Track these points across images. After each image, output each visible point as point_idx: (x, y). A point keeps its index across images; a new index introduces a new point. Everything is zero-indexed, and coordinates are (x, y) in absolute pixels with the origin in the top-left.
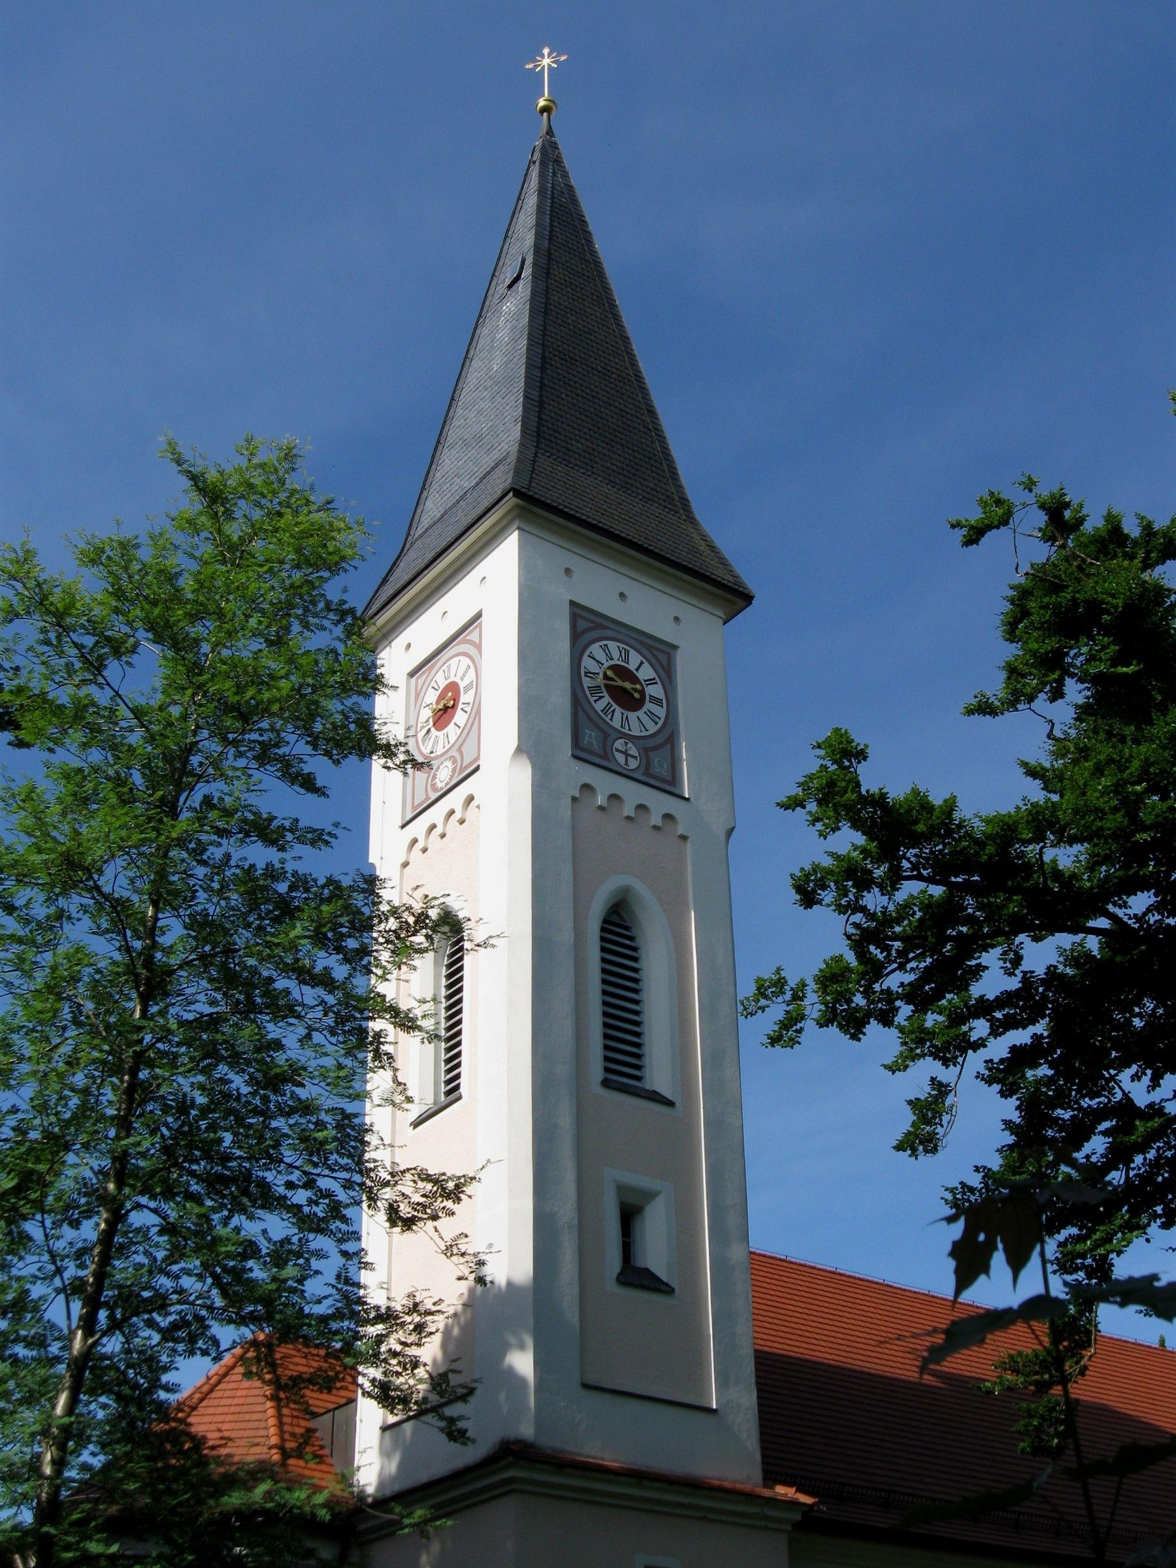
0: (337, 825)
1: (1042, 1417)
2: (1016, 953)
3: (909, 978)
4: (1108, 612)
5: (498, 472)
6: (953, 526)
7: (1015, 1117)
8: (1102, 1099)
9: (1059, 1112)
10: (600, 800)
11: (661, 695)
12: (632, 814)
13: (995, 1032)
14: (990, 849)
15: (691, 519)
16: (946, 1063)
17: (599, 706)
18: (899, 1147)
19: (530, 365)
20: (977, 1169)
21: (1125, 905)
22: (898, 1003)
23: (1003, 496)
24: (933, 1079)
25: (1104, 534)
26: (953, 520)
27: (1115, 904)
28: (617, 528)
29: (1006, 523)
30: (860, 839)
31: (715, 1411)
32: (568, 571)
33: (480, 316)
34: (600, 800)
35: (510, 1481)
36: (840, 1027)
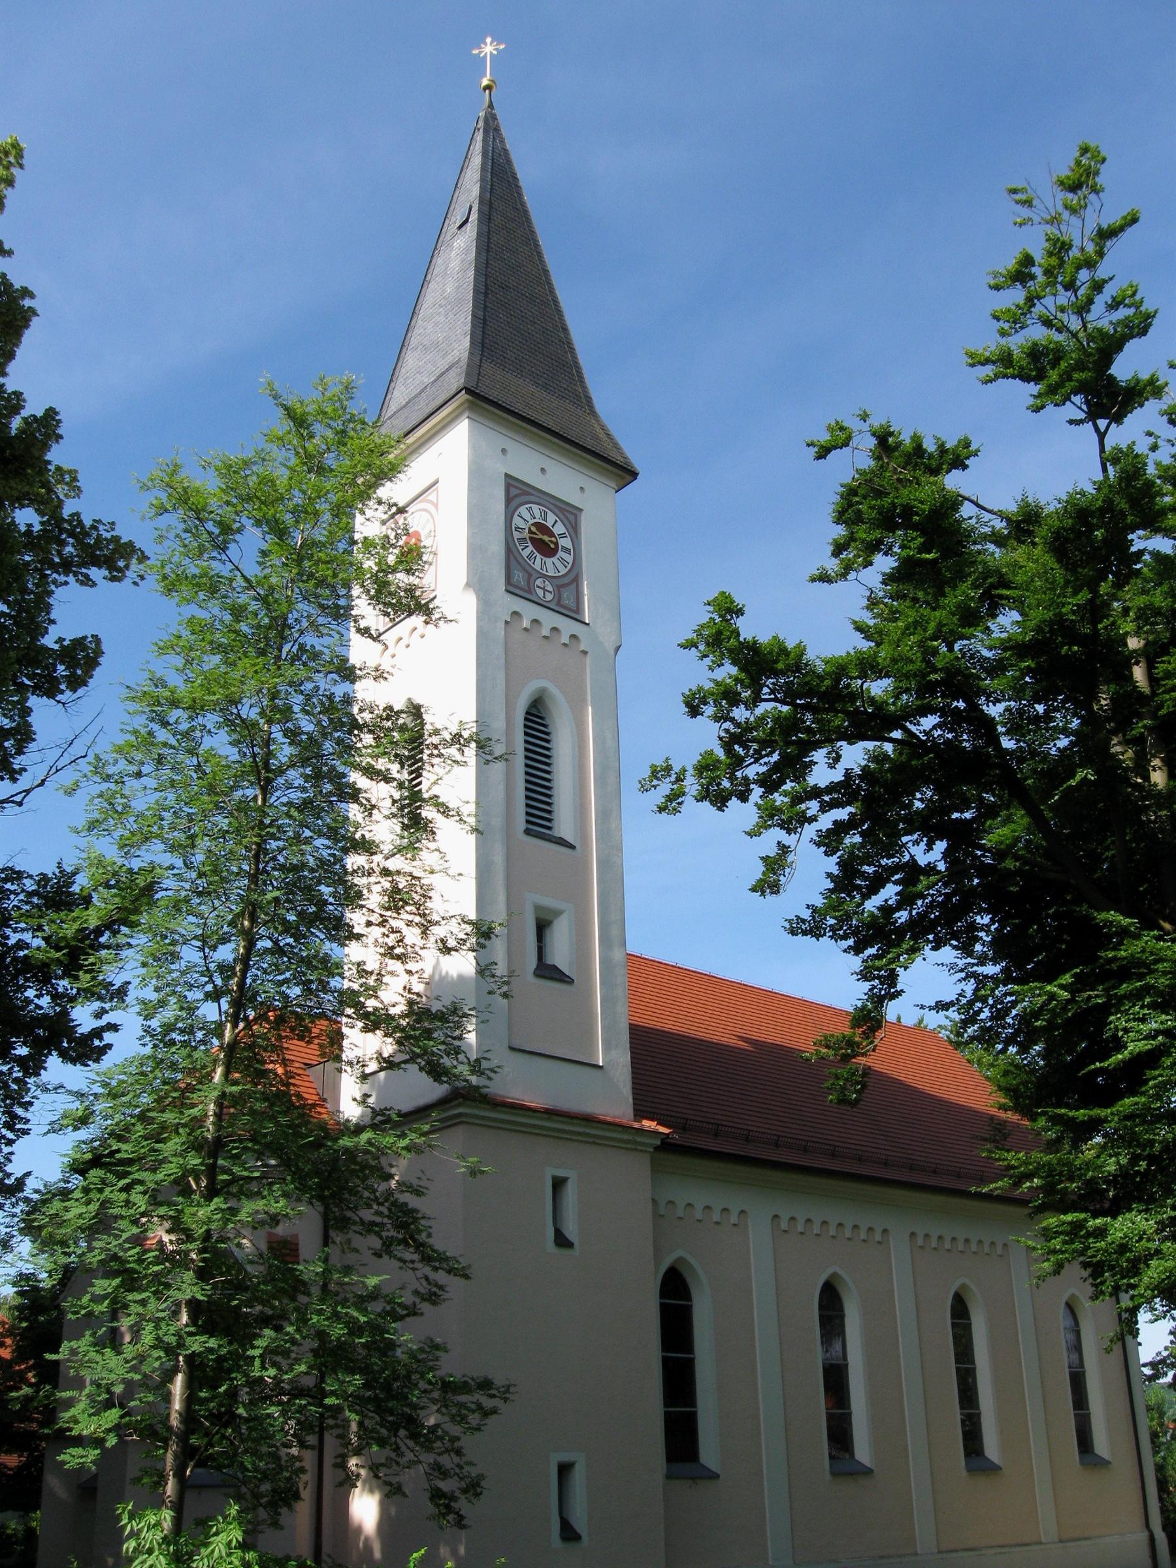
0: (393, 667)
1: (846, 1080)
2: (837, 753)
4: (917, 514)
5: (452, 373)
6: (808, 445)
7: (835, 870)
9: (865, 868)
10: (526, 623)
11: (570, 546)
12: (567, 642)
14: (827, 682)
15: (593, 412)
16: (789, 832)
17: (525, 553)
18: (753, 890)
19: (476, 291)
20: (808, 907)
21: (918, 724)
22: (752, 786)
23: (845, 424)
24: (779, 843)
25: (910, 450)
26: (809, 440)
27: (911, 722)
28: (543, 419)
29: (847, 445)
30: (734, 670)
31: (601, 1067)
32: (504, 451)
33: (435, 248)
34: (526, 623)
35: (460, 1115)
36: (711, 802)
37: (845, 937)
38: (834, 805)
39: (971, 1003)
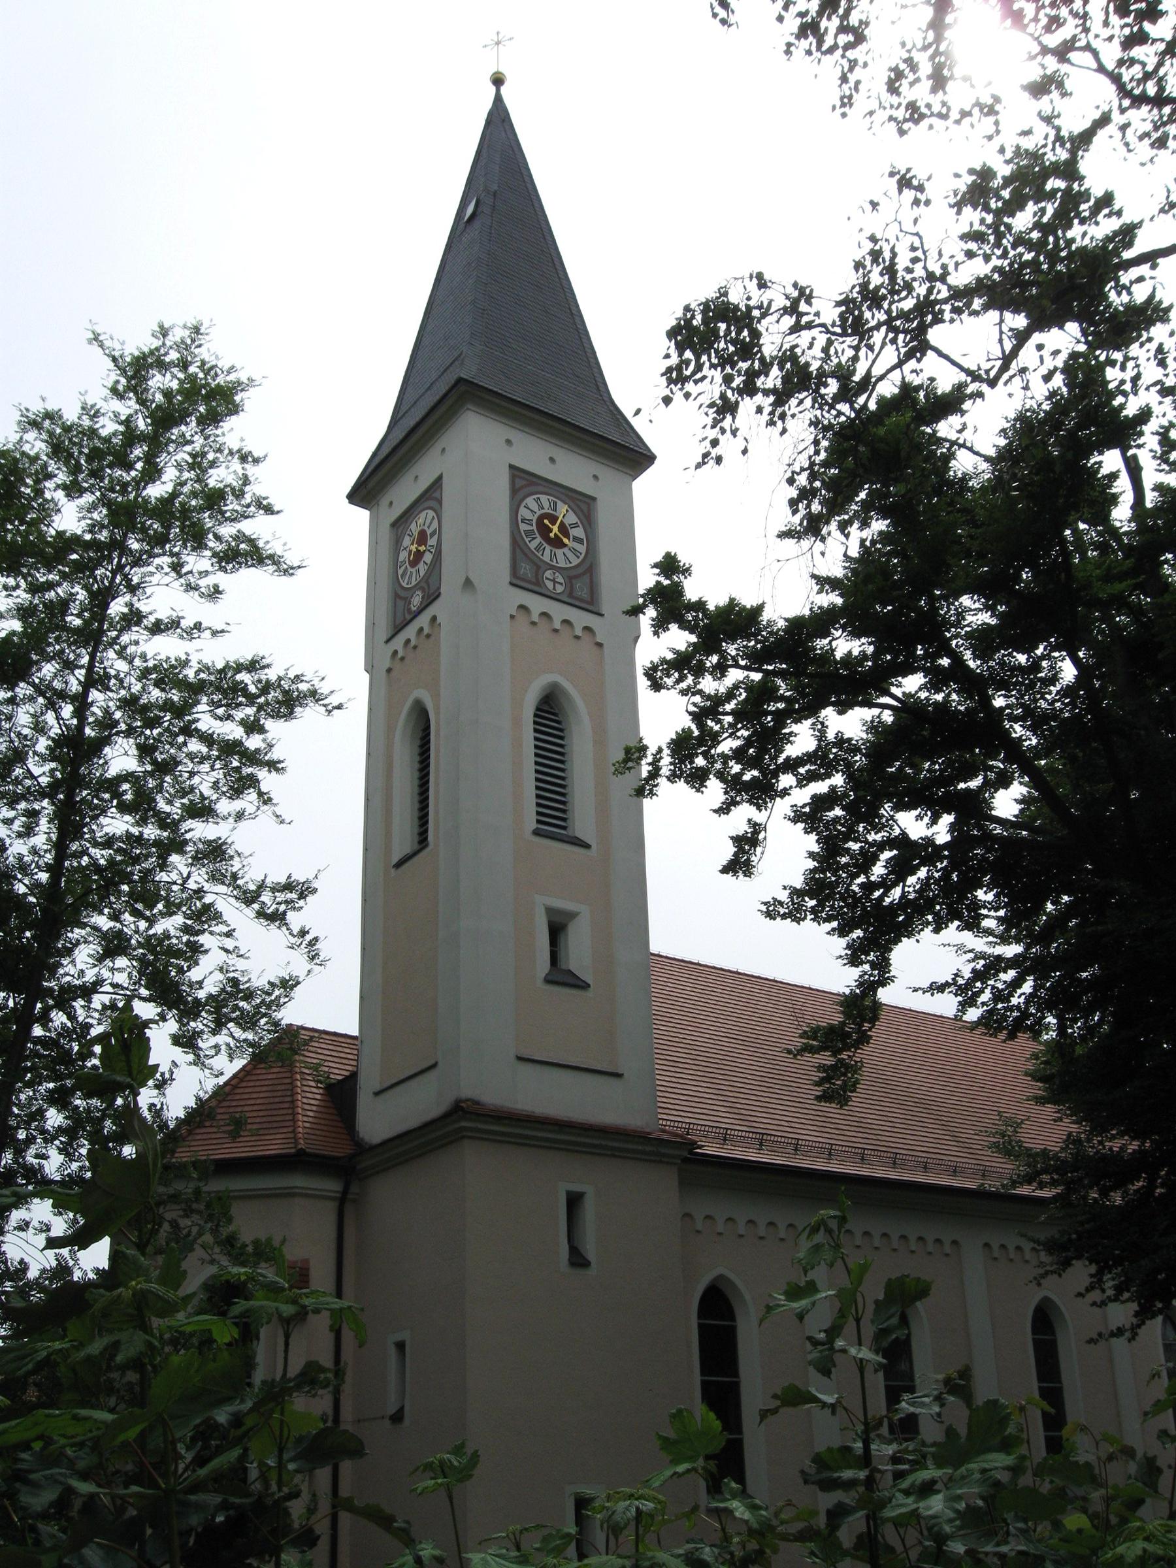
2: (822, 724)
3: (736, 744)
7: (816, 848)
8: (883, 834)
13: (800, 785)
16: (759, 808)
18: (725, 870)
24: (749, 821)
37: (828, 919)
38: (812, 777)
39: (969, 984)
